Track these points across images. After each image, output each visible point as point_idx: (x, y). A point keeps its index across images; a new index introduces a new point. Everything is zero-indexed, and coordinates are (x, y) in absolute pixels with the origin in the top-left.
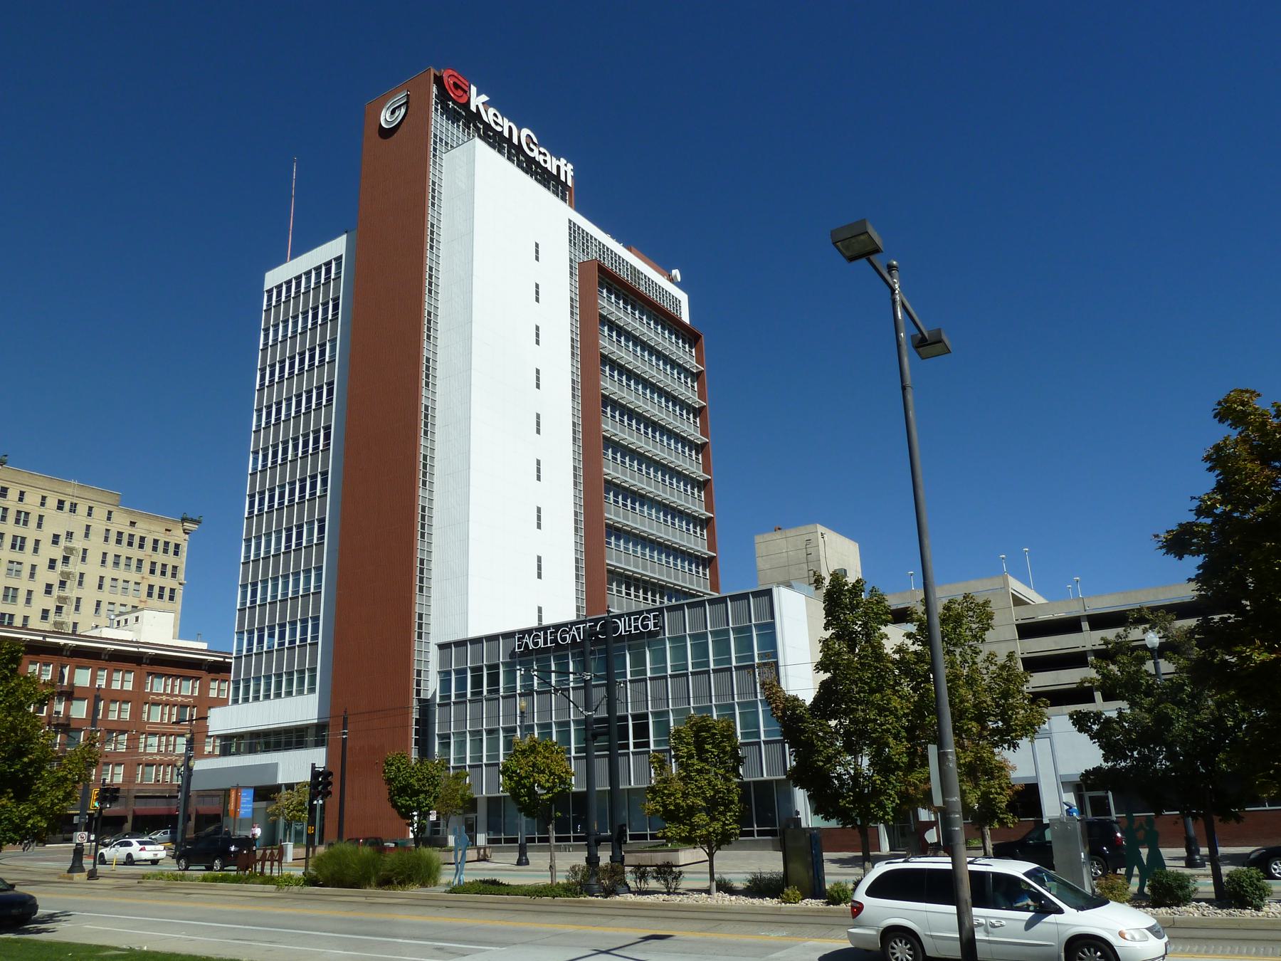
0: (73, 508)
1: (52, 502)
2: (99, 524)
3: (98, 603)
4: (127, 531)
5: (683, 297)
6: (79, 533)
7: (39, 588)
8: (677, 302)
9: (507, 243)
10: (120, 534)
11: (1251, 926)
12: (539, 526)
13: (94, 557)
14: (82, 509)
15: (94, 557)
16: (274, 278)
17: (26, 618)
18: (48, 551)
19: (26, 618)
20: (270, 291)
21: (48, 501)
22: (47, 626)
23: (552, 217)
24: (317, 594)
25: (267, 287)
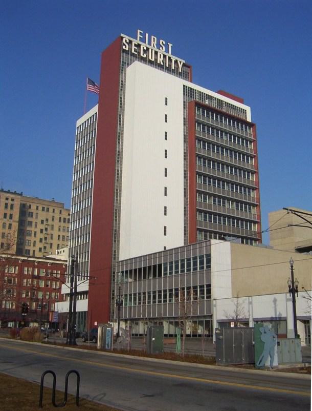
0: (48, 210)
1: (40, 208)
2: (57, 216)
3: (58, 245)
4: (67, 217)
5: (248, 109)
6: (50, 219)
7: (38, 240)
8: (244, 112)
9: (154, 104)
10: (65, 219)
11: (120, 315)
12: (165, 214)
13: (56, 228)
14: (51, 210)
15: (56, 228)
16: (79, 122)
17: (34, 251)
18: (40, 226)
19: (34, 251)
20: (78, 128)
21: (39, 208)
22: (40, 255)
23: (173, 87)
24: (89, 243)
25: (77, 127)
